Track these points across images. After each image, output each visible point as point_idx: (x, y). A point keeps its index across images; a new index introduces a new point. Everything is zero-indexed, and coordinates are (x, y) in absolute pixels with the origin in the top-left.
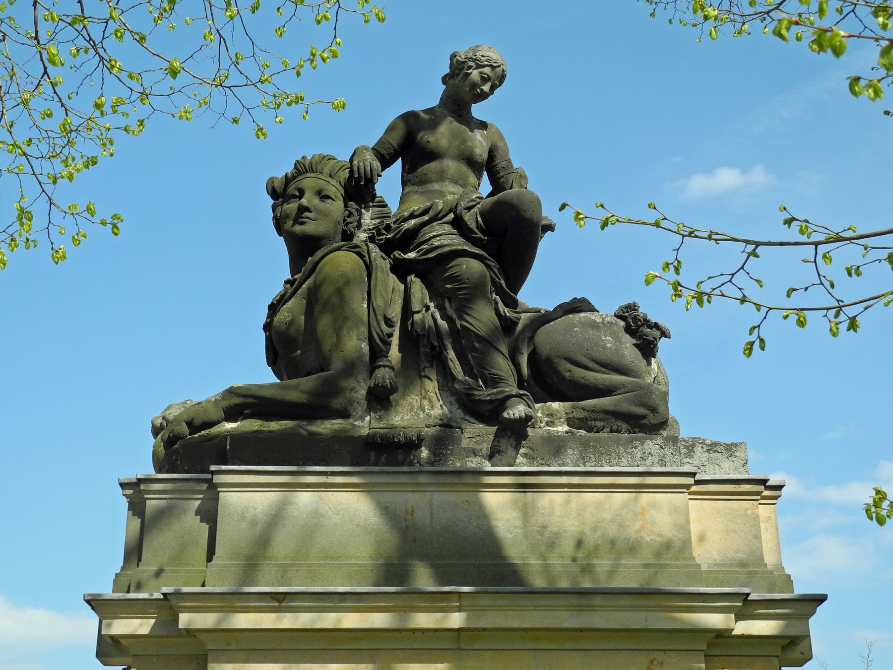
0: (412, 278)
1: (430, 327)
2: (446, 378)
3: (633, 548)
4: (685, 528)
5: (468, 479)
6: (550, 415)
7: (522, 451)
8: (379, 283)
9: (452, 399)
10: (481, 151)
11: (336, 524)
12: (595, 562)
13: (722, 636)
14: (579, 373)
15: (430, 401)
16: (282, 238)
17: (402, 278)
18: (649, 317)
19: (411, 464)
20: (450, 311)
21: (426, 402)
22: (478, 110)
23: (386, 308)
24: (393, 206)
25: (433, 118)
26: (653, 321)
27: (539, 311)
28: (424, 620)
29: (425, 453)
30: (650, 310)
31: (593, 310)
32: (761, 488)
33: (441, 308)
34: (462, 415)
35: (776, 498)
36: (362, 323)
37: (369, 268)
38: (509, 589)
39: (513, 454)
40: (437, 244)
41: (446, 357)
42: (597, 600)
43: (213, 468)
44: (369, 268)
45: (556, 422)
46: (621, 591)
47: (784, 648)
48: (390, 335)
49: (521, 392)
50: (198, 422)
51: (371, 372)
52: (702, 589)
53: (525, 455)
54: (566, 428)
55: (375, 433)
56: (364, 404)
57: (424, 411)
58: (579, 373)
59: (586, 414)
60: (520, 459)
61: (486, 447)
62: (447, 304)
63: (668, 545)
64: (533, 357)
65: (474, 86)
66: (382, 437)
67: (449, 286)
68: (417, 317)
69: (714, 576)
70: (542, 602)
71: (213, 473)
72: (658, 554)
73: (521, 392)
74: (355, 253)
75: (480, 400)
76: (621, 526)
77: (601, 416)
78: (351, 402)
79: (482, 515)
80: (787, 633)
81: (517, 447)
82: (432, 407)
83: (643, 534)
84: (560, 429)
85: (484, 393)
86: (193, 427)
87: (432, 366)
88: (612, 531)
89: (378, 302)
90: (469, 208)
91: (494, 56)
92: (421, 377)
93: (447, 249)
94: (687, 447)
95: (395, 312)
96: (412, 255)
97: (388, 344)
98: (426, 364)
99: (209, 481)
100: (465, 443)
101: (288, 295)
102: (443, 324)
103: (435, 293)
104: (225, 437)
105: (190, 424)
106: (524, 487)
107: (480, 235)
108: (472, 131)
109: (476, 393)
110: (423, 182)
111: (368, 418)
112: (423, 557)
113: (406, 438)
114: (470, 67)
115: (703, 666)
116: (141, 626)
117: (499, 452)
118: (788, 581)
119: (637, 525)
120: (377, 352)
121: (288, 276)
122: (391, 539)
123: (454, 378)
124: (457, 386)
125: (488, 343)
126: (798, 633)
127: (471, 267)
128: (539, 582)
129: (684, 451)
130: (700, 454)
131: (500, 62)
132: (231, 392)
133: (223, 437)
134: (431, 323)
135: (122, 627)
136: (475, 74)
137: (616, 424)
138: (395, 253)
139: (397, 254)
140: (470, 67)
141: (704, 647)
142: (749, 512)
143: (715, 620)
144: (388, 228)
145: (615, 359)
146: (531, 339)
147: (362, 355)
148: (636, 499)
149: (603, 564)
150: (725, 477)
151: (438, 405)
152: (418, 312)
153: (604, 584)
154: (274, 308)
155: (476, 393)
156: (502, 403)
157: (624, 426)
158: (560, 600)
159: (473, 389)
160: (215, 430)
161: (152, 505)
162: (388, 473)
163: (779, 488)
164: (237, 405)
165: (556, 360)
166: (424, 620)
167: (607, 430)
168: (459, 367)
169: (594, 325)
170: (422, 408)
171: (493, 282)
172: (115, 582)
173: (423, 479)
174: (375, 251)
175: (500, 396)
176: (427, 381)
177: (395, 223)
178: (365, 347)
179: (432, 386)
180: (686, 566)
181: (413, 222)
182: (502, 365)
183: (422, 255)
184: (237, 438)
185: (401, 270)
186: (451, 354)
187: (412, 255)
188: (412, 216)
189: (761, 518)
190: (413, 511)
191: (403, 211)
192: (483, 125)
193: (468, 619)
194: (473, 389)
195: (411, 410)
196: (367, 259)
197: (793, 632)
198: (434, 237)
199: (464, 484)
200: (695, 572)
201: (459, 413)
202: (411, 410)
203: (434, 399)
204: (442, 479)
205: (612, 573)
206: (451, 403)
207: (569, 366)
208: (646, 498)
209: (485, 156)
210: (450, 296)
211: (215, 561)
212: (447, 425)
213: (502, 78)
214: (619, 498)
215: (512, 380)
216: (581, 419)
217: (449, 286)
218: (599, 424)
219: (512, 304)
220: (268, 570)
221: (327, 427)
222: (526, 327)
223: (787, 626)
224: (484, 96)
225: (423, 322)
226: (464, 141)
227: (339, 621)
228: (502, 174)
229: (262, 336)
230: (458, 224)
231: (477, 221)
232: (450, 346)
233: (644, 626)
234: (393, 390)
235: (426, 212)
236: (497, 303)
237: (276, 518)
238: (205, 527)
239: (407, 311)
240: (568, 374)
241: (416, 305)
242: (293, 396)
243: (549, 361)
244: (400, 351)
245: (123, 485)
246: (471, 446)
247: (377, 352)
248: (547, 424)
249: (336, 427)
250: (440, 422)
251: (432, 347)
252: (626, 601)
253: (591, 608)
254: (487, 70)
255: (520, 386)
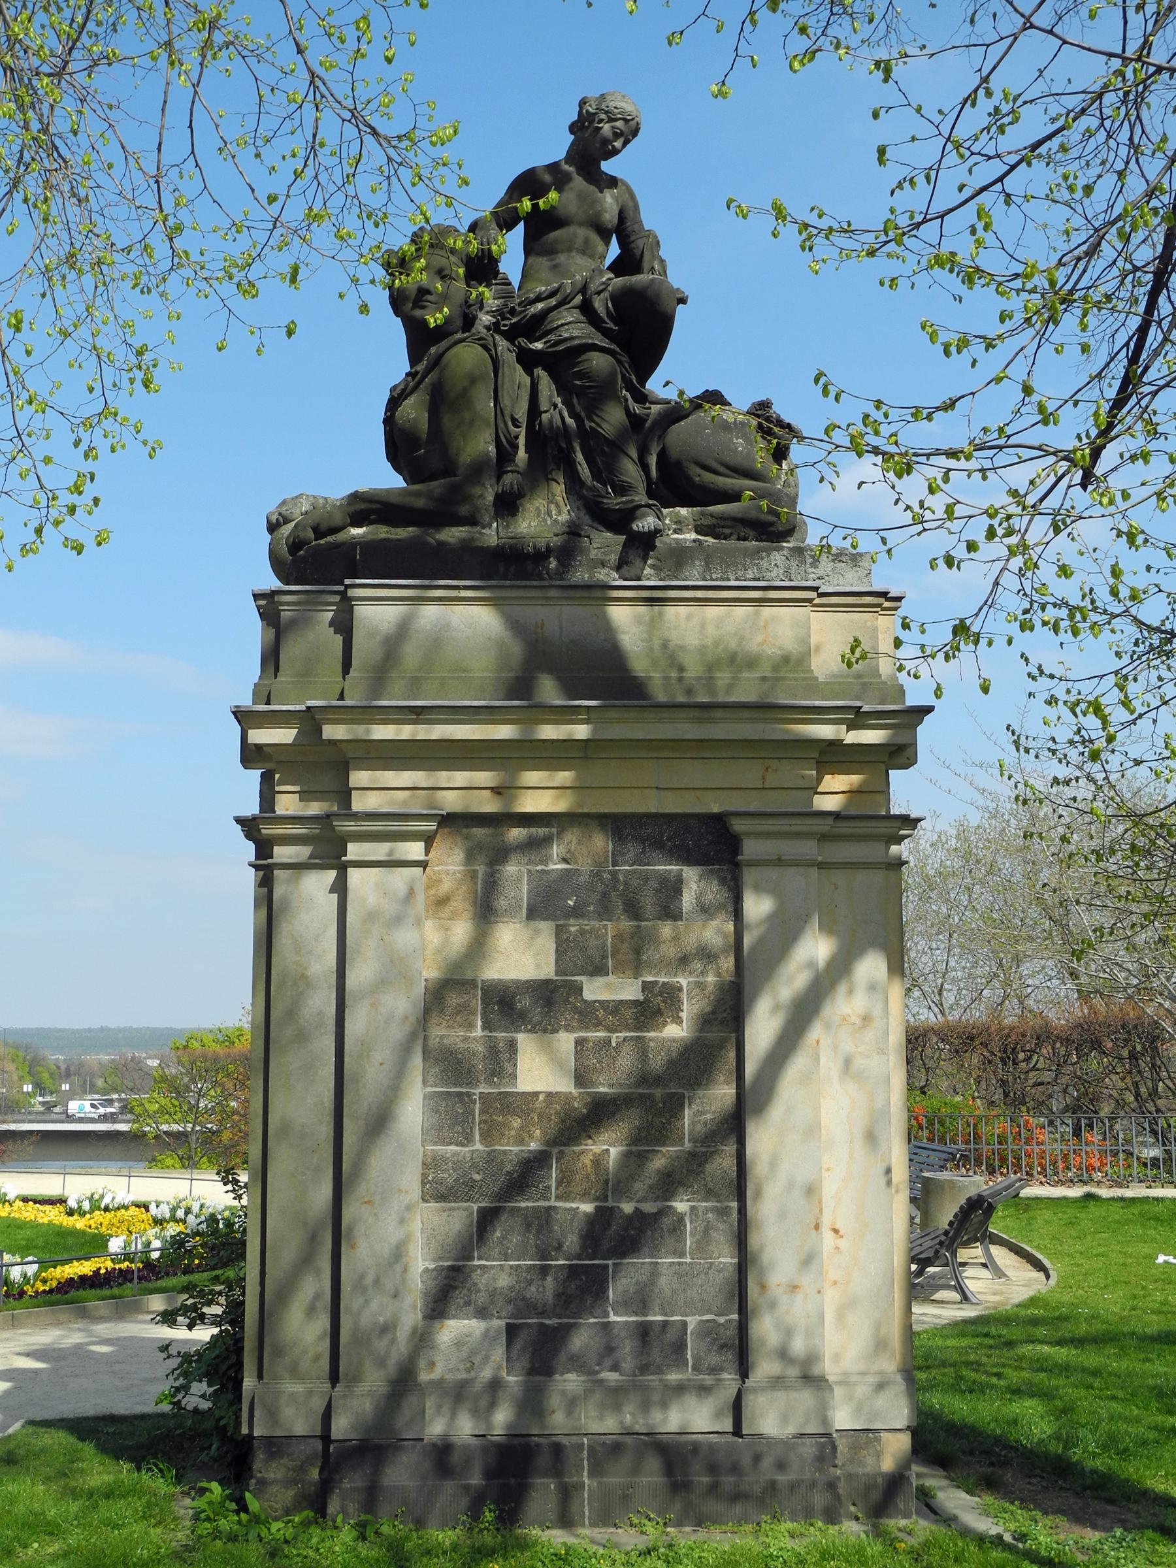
0: (539, 372)
1: (558, 427)
2: (574, 485)
3: (751, 662)
4: (805, 641)
5: (598, 593)
6: (678, 522)
7: (649, 562)
8: (506, 380)
9: (579, 503)
10: (610, 216)
11: (468, 637)
12: (718, 675)
13: (834, 745)
14: (709, 477)
15: (558, 506)
16: (399, 319)
17: (529, 370)
18: (782, 417)
19: (541, 578)
20: (578, 409)
21: (553, 507)
22: (608, 166)
23: (513, 408)
24: (515, 279)
25: (556, 175)
26: (787, 420)
27: (669, 403)
28: (549, 732)
29: (553, 564)
30: (783, 410)
31: (725, 403)
32: (881, 600)
33: (568, 403)
34: (589, 522)
35: (896, 609)
36: (488, 424)
37: (496, 363)
38: (636, 702)
39: (641, 565)
40: (566, 335)
41: (574, 461)
42: (719, 714)
43: (347, 582)
44: (496, 363)
45: (684, 529)
46: (264, 960)
47: (892, 754)
48: (517, 437)
49: (651, 502)
50: (324, 526)
51: (499, 478)
52: (817, 703)
53: (653, 566)
54: (693, 536)
55: (504, 544)
56: (492, 510)
57: (551, 517)
58: (709, 477)
59: (714, 521)
60: (648, 571)
61: (613, 558)
62: (575, 401)
63: (786, 659)
64: (662, 456)
65: (606, 142)
66: (512, 547)
67: (578, 383)
68: (545, 417)
69: (833, 687)
70: (666, 715)
71: (347, 587)
72: (776, 668)
73: (651, 502)
74: (481, 345)
75: (609, 509)
76: (742, 638)
77: (728, 523)
78: (477, 509)
79: (608, 629)
80: (895, 742)
81: (645, 559)
82: (560, 513)
83: (764, 647)
84: (688, 536)
85: (614, 502)
86: (319, 532)
87: (559, 469)
88: (733, 645)
89: (506, 401)
90: (599, 293)
91: (628, 107)
92: (548, 480)
93: (577, 342)
94: (812, 557)
95: (522, 413)
96: (539, 345)
97: (516, 447)
98: (553, 466)
99: (343, 594)
100: (593, 554)
101: (409, 388)
102: (570, 421)
103: (563, 388)
104: (356, 544)
105: (316, 529)
106: (650, 601)
107: (611, 325)
108: (601, 192)
109: (605, 501)
110: (550, 251)
111: (495, 525)
112: (551, 671)
113: (483, 484)
114: (601, 121)
115: (814, 772)
116: (284, 736)
117: (627, 563)
118: (901, 692)
119: (759, 638)
120: (505, 454)
121: (408, 369)
122: (517, 649)
123: (582, 483)
124: (585, 492)
125: (616, 447)
126: (904, 742)
127: (599, 362)
128: (662, 698)
129: (810, 560)
130: (825, 564)
131: (634, 114)
132: (355, 497)
133: (353, 544)
134: (559, 422)
135: (258, 736)
136: (606, 128)
137: (744, 531)
138: (520, 339)
139: (522, 341)
140: (601, 121)
141: (816, 755)
142: (869, 623)
143: (825, 731)
144: (513, 312)
145: (745, 464)
146: (662, 437)
147: (489, 459)
148: (757, 614)
149: (723, 677)
150: (848, 589)
151: (565, 509)
152: (546, 412)
153: (721, 698)
154: (394, 403)
155: (605, 501)
156: (631, 514)
157: (752, 533)
158: (682, 714)
159: (602, 496)
160: (341, 537)
161: (285, 615)
162: (518, 587)
163: (899, 599)
164: (362, 511)
165: (686, 464)
166: (549, 732)
167: (735, 537)
168: (587, 471)
169: (726, 426)
170: (549, 514)
171: (623, 377)
172: (254, 693)
173: (553, 593)
174: (502, 344)
175: (631, 505)
176: (554, 484)
177: (520, 304)
178: (492, 449)
179: (559, 489)
180: (804, 679)
181: (540, 306)
182: (630, 470)
183: (551, 347)
184: (369, 547)
185: (528, 360)
186: (580, 457)
187: (539, 345)
188: (538, 299)
189: (880, 629)
190: (543, 625)
191: (528, 291)
192: (613, 182)
193: (594, 731)
194: (602, 496)
195: (538, 516)
196: (493, 352)
197: (900, 740)
198: (563, 325)
199: (593, 598)
200: (813, 686)
201: (586, 519)
202: (538, 516)
203: (561, 503)
204: (571, 593)
205: (730, 688)
206: (578, 509)
207: (699, 470)
208: (767, 611)
209: (616, 220)
210: (580, 392)
211: (353, 673)
212: (573, 532)
213: (635, 132)
214: (741, 611)
215: (642, 489)
216: (708, 526)
217: (578, 383)
218: (727, 531)
219: (642, 398)
220: (397, 684)
221: (453, 535)
222: (656, 423)
223: (893, 735)
224: (615, 152)
225: (551, 421)
226: (594, 202)
227: (398, 732)
228: (633, 238)
229: (381, 429)
230: (586, 308)
231: (607, 308)
232: (578, 448)
233: (761, 737)
234: (520, 495)
235: (553, 294)
236: (626, 400)
237: (403, 629)
238: (339, 639)
239: (534, 409)
240: (697, 479)
241: (544, 405)
242: (420, 503)
243: (678, 464)
244: (526, 452)
245: (256, 597)
246: (599, 556)
247: (505, 454)
248: (675, 532)
249: (464, 535)
250: (567, 530)
251: (560, 449)
252: (746, 714)
253: (712, 720)
254: (619, 124)
255: (650, 494)
